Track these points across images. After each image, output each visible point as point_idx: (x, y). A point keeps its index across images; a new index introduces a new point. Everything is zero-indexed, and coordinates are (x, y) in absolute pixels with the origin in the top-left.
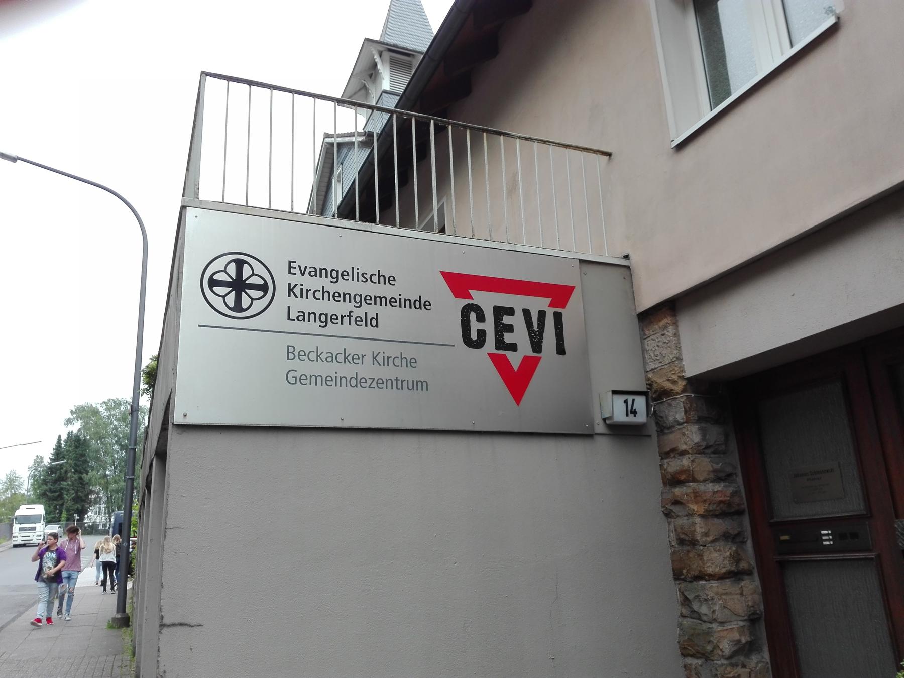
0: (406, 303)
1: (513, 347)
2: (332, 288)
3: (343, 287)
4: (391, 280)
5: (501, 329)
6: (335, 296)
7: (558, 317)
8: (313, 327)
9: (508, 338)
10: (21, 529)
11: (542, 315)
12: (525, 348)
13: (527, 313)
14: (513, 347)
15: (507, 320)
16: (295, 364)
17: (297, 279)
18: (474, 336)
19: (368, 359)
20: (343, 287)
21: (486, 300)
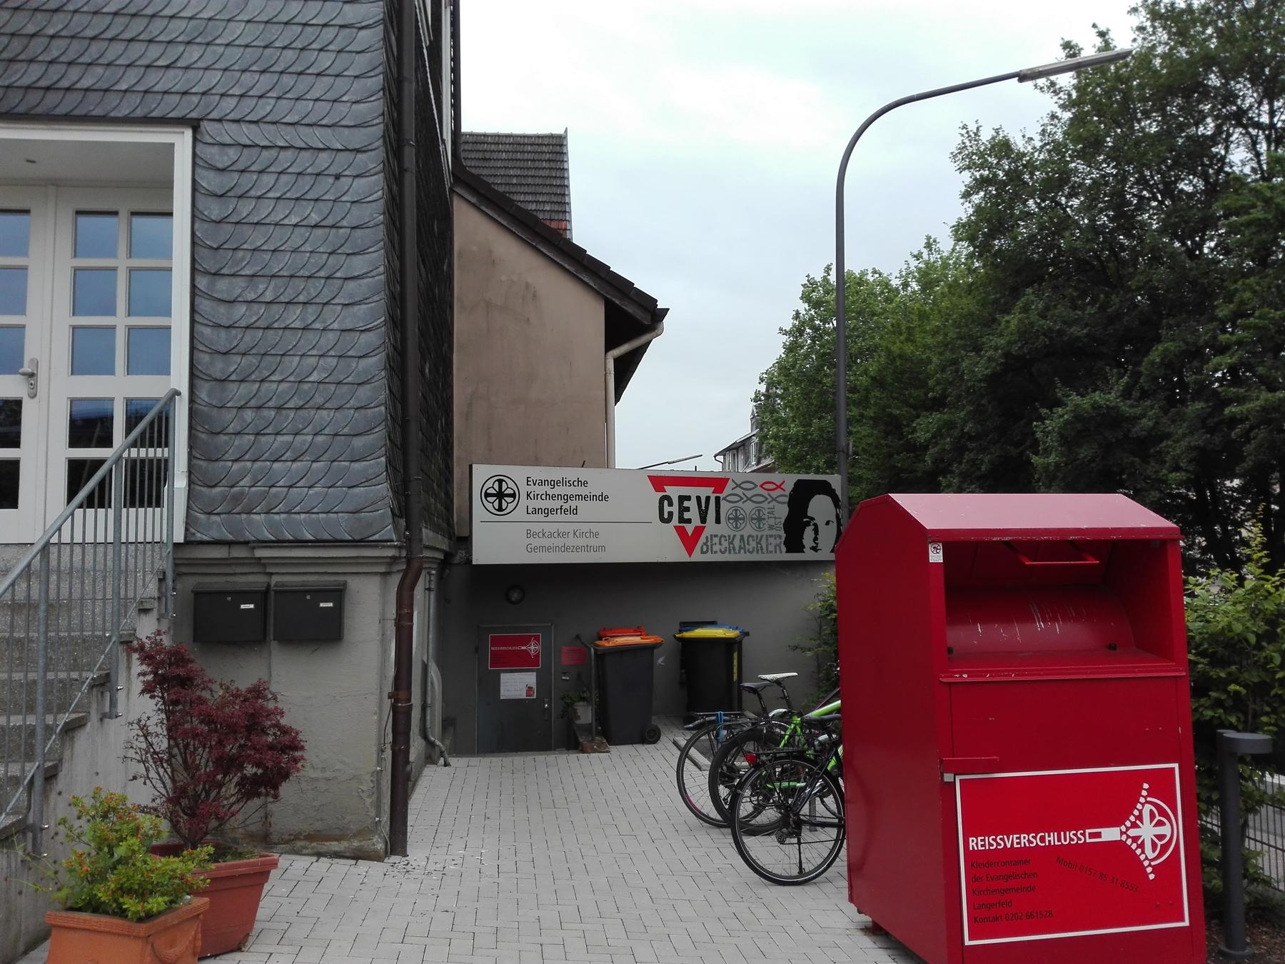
0: (594, 497)
1: (689, 521)
2: (551, 492)
3: (559, 490)
4: (585, 483)
5: (683, 509)
6: (553, 497)
7: (718, 499)
8: (541, 517)
9: (686, 515)
10: (815, 549)
11: (708, 498)
12: (696, 521)
13: (698, 498)
14: (689, 521)
15: (686, 504)
16: (531, 540)
17: (530, 489)
18: (666, 516)
19: (571, 534)
20: (559, 490)
21: (674, 492)
